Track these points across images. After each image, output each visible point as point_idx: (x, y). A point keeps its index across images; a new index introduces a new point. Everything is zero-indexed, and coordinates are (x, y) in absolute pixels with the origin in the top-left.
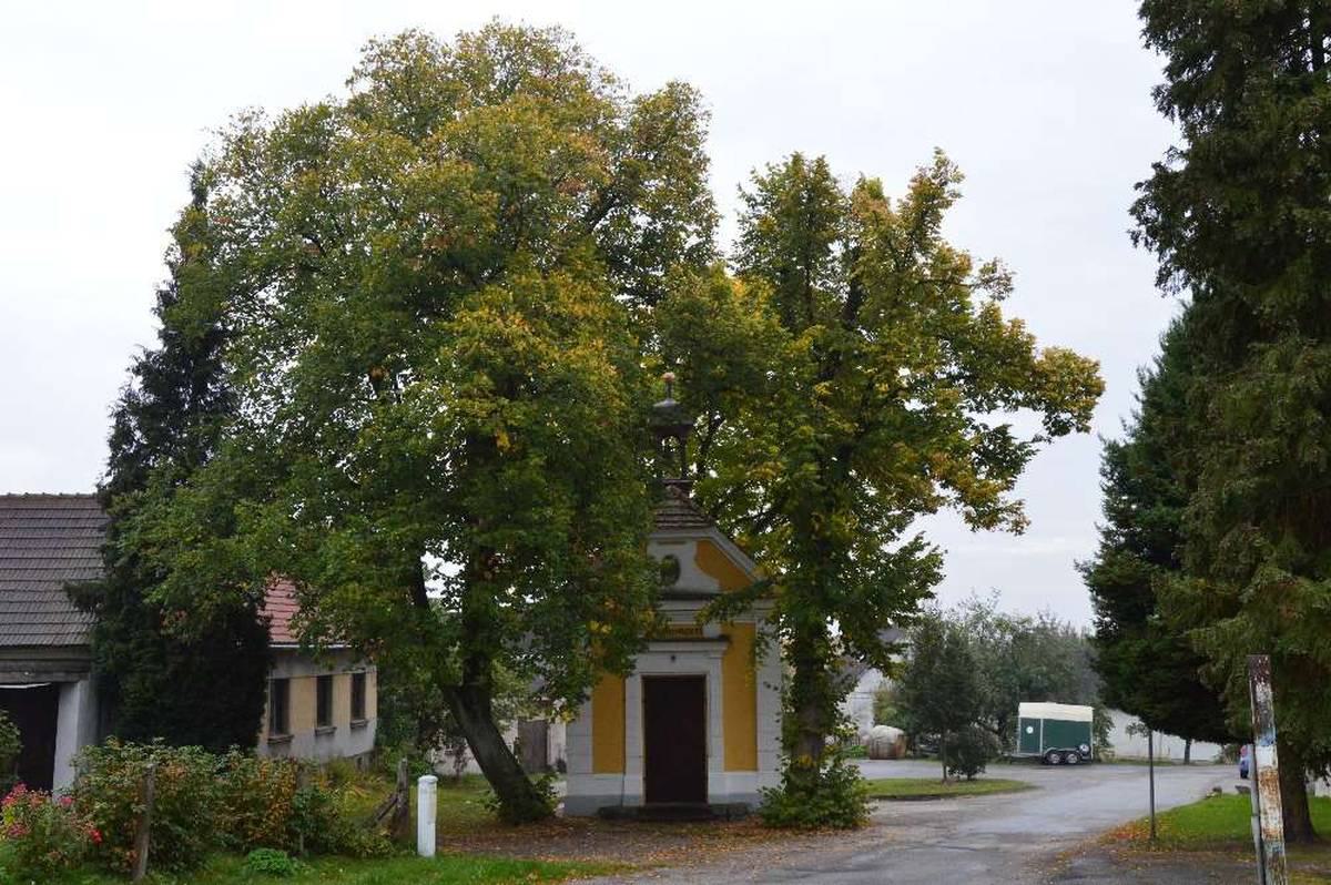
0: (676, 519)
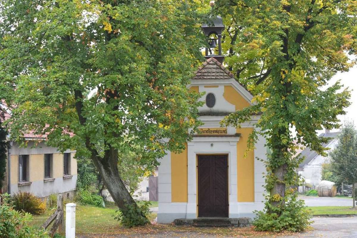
0: (214, 74)
